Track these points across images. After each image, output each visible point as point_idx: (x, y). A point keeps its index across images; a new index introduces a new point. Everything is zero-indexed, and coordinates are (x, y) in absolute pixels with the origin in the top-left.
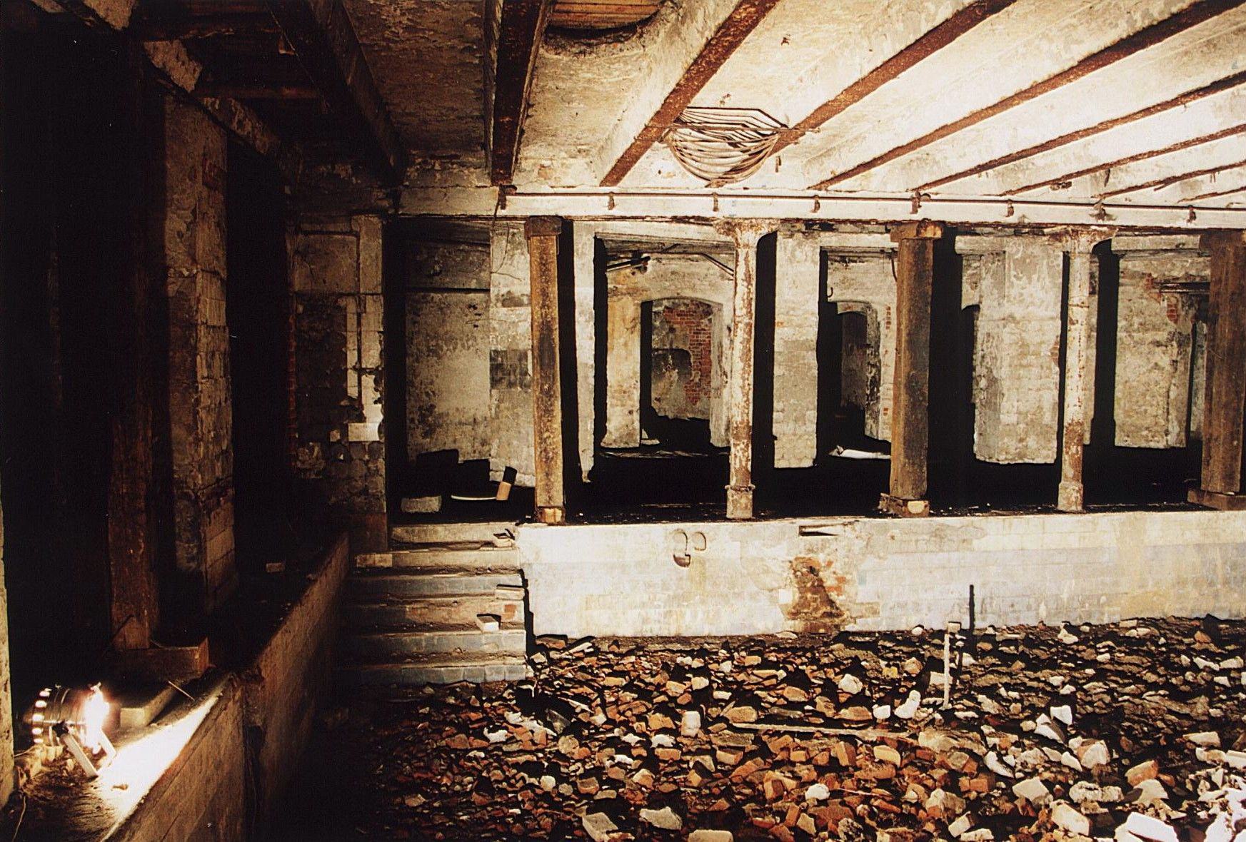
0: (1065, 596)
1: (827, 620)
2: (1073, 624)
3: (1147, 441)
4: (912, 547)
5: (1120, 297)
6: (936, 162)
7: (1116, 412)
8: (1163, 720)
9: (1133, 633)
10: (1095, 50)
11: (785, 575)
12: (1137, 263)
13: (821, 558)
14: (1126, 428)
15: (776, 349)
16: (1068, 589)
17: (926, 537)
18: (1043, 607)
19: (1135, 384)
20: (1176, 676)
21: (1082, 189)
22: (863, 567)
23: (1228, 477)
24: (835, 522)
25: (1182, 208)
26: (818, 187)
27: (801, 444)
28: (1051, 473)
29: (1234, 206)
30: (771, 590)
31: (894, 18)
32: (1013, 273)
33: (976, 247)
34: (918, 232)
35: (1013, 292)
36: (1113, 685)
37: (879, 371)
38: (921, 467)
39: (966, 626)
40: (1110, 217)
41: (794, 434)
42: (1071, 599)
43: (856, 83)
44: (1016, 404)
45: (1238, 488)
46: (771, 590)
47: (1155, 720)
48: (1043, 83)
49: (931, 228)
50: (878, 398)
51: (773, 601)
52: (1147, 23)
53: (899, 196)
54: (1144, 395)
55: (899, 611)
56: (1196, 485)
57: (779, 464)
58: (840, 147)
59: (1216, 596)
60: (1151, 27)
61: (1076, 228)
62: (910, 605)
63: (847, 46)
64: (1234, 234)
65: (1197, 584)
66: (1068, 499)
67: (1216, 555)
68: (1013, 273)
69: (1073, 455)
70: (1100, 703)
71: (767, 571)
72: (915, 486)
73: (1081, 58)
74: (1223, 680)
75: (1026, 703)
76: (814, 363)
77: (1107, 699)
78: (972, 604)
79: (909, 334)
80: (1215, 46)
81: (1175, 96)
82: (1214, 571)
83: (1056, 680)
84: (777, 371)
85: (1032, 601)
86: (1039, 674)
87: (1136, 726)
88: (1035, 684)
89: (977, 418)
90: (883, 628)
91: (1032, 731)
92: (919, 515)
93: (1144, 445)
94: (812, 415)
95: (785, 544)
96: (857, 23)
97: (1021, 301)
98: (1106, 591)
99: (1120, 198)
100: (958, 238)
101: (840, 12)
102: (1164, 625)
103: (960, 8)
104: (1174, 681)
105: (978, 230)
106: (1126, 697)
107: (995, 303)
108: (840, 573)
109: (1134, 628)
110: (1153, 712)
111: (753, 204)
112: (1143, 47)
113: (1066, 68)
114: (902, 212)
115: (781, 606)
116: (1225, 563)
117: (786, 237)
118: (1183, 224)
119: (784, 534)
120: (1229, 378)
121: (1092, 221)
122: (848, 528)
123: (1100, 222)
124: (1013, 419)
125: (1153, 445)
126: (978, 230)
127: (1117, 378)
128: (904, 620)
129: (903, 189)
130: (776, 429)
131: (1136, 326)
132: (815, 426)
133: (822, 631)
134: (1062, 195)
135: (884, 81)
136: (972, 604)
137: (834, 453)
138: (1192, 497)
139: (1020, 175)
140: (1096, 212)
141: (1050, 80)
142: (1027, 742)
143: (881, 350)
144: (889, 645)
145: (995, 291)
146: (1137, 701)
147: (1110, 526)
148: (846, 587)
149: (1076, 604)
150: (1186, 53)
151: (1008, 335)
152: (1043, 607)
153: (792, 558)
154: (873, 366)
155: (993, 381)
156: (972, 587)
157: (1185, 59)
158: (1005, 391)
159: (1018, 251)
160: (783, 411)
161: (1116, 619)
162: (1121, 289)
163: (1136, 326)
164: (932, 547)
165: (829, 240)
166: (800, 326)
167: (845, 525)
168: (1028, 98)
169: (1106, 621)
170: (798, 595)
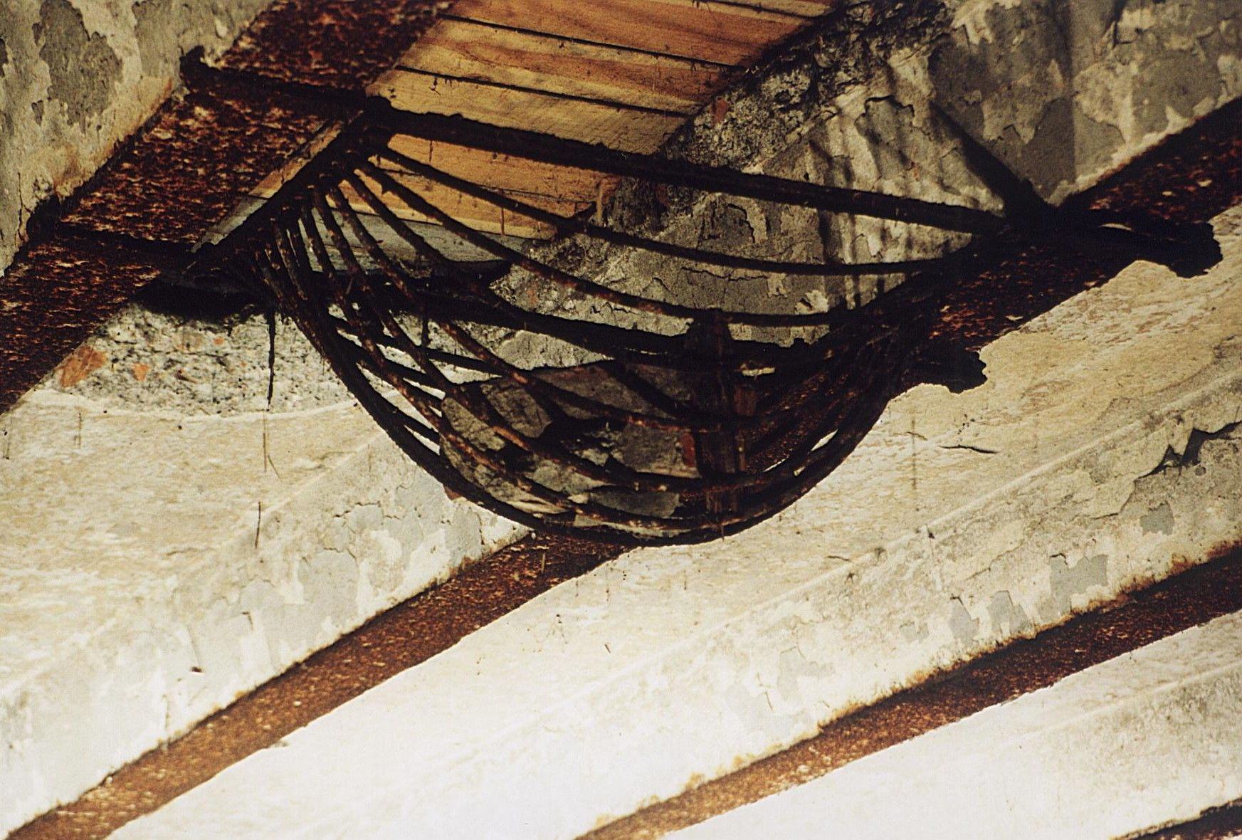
10: (869, 698)
31: (277, 565)
43: (151, 756)
52: (1006, 633)
60: (1019, 644)
63: (126, 638)
73: (827, 716)
80: (1203, 706)
96: (162, 573)
101: (109, 538)
103: (475, 554)
112: (1000, 699)
113: (787, 742)
125: (564, 343)
135: (238, 754)
141: (741, 773)
142: (814, 114)
150: (1127, 719)
157: (1124, 736)
168: (677, 823)
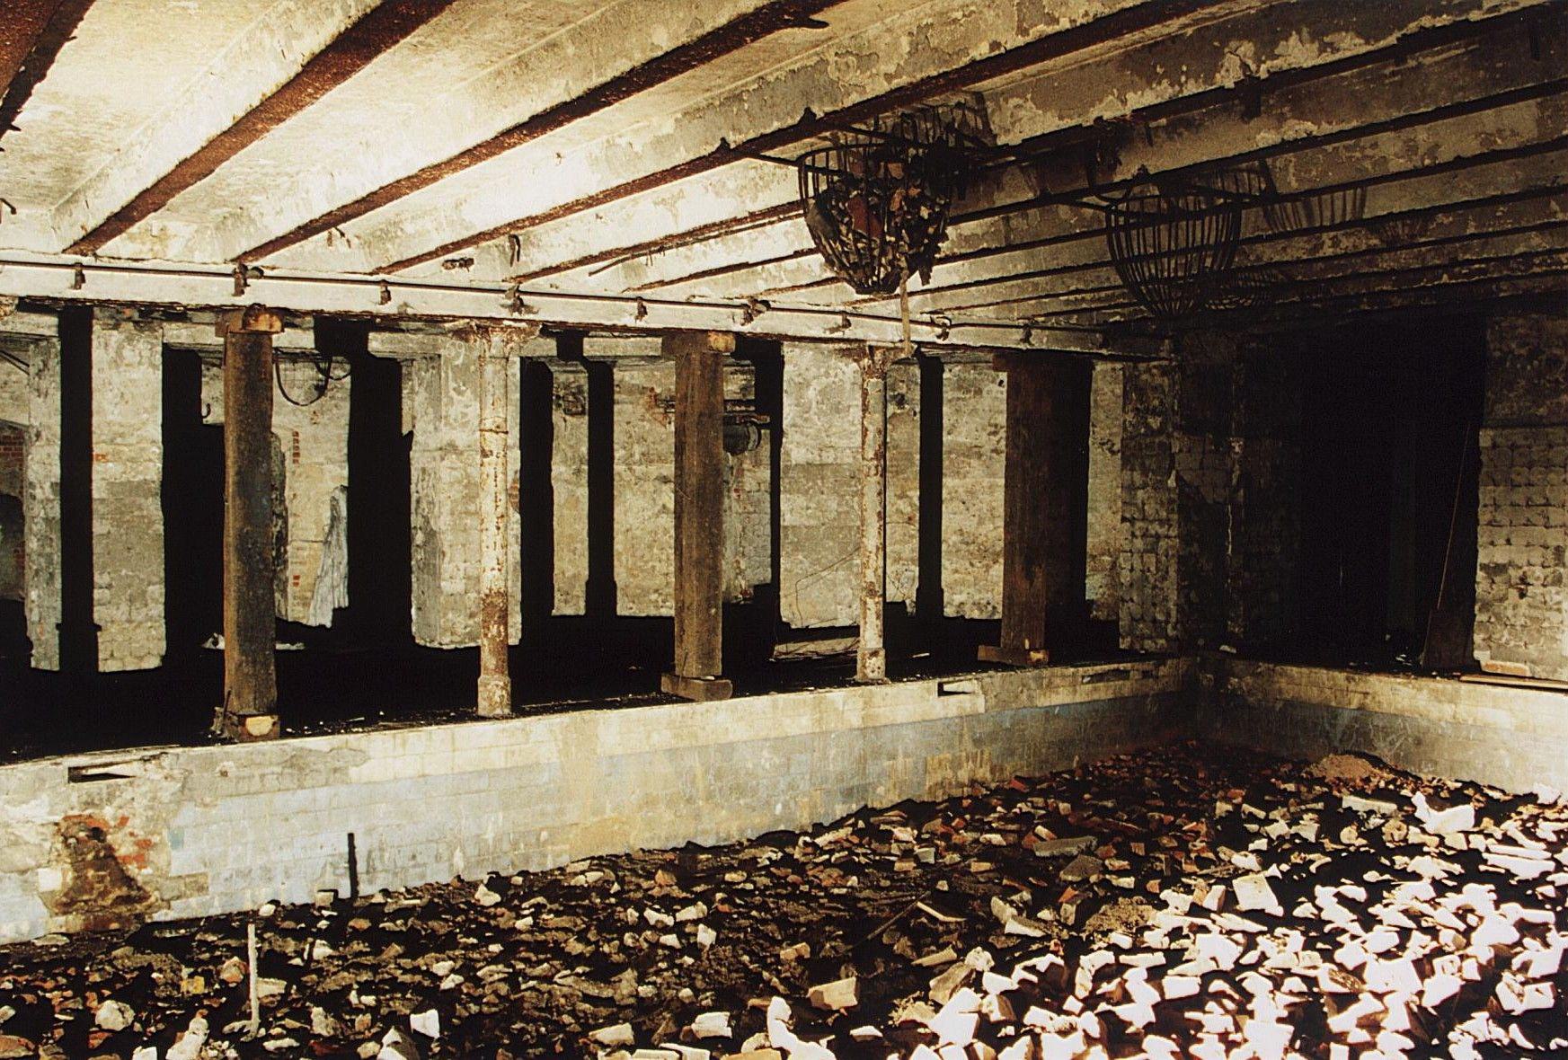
0: (490, 836)
1: (123, 909)
2: (503, 874)
3: (657, 607)
4: (256, 784)
5: (616, 418)
6: (252, 221)
7: (616, 570)
8: (573, 1013)
9: (581, 880)
11: (47, 845)
12: (635, 373)
13: (108, 813)
14: (630, 592)
15: (95, 495)
16: (493, 826)
17: (278, 769)
18: (458, 853)
19: (638, 533)
20: (609, 941)
21: (489, 267)
22: (175, 823)
23: (706, 657)
24: (128, 758)
25: (628, 299)
26: (76, 247)
27: (140, 634)
28: (468, 660)
29: (697, 300)
30: (23, 872)
32: (452, 385)
33: (398, 348)
34: (245, 324)
35: (454, 411)
36: (520, 966)
37: (286, 522)
38: (268, 666)
39: (345, 893)
40: (529, 310)
41: (130, 621)
42: (498, 840)
44: (462, 566)
45: (719, 671)
46: (23, 872)
47: (560, 1014)
48: (273, 96)
49: (264, 318)
50: (286, 562)
51: (28, 888)
53: (213, 269)
54: (650, 547)
55: (241, 883)
56: (670, 669)
57: (107, 665)
58: (84, 190)
59: (697, 817)
61: (483, 323)
62: (256, 873)
64: (699, 336)
65: (671, 803)
66: (490, 699)
67: (694, 762)
68: (452, 385)
69: (493, 638)
70: (492, 998)
71: (16, 843)
72: (259, 694)
74: (671, 940)
75: (384, 1011)
76: (158, 515)
77: (504, 989)
78: (352, 861)
79: (238, 473)
81: (493, 135)
82: (693, 782)
83: (441, 968)
84: (98, 527)
85: (442, 848)
86: (420, 961)
87: (531, 1028)
88: (407, 978)
89: (415, 586)
90: (215, 911)
91: (611, 999)
92: (265, 738)
93: (653, 612)
94: (157, 591)
95: (44, 797)
97: (465, 425)
98: (549, 823)
99: (542, 283)
100: (371, 335)
102: (627, 865)
104: (606, 949)
105: (403, 325)
106: (532, 983)
107: (431, 428)
108: (141, 835)
109: (583, 873)
110: (563, 1001)
111: (350, 291)
114: (220, 292)
115: (42, 895)
116: (707, 772)
117: (106, 327)
118: (631, 322)
119: (43, 781)
120: (701, 526)
121: (505, 313)
122: (151, 766)
123: (516, 315)
124: (459, 586)
126: (403, 325)
127: (616, 526)
128: (248, 894)
129: (220, 260)
130: (99, 614)
131: (637, 457)
132: (162, 608)
133: (114, 926)
134: (459, 276)
136: (352, 861)
137: (209, 645)
138: (666, 685)
139: (389, 246)
140: (510, 302)
143: (287, 493)
144: (211, 938)
145: (430, 410)
146: (545, 987)
147: (547, 734)
148: (152, 855)
149: (506, 846)
151: (447, 471)
152: (458, 853)
153: (58, 818)
154: (279, 516)
155: (431, 535)
156: (351, 836)
157: (498, 82)
158: (446, 549)
159: (458, 356)
160: (109, 587)
161: (563, 861)
162: (616, 408)
163: (637, 457)
164: (287, 782)
165: (178, 334)
166: (132, 460)
167: (145, 760)
169: (550, 866)
170: (70, 875)
